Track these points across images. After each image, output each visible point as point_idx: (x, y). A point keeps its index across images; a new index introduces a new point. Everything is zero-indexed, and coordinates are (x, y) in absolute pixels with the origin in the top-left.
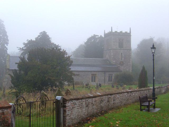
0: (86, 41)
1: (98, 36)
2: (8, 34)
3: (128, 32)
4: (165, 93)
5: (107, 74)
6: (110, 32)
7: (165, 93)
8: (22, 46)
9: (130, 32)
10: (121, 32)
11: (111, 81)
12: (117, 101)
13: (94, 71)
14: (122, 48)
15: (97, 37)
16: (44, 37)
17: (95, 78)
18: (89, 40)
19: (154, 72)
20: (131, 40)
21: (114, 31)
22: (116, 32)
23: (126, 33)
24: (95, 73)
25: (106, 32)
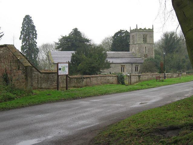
0: (113, 34)
1: (124, 31)
2: (36, 29)
3: (151, 28)
4: (175, 77)
5: (134, 65)
6: (135, 29)
7: (175, 77)
8: (57, 41)
9: (153, 29)
10: (145, 29)
11: (137, 71)
12: (146, 78)
13: (124, 63)
14: (146, 42)
15: (123, 32)
16: (76, 33)
17: (123, 68)
18: (116, 34)
19: (62, 63)
20: (153, 36)
21: (138, 28)
22: (140, 29)
23: (149, 29)
24: (124, 65)
25: (132, 29)
